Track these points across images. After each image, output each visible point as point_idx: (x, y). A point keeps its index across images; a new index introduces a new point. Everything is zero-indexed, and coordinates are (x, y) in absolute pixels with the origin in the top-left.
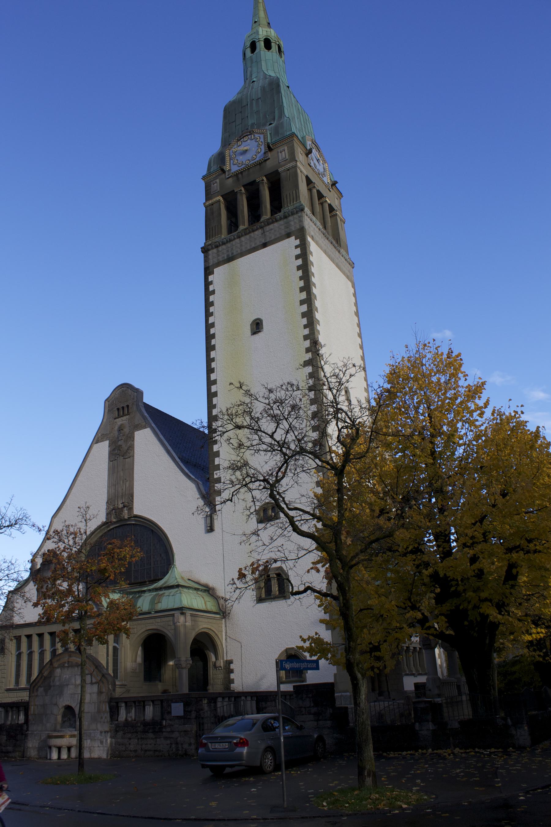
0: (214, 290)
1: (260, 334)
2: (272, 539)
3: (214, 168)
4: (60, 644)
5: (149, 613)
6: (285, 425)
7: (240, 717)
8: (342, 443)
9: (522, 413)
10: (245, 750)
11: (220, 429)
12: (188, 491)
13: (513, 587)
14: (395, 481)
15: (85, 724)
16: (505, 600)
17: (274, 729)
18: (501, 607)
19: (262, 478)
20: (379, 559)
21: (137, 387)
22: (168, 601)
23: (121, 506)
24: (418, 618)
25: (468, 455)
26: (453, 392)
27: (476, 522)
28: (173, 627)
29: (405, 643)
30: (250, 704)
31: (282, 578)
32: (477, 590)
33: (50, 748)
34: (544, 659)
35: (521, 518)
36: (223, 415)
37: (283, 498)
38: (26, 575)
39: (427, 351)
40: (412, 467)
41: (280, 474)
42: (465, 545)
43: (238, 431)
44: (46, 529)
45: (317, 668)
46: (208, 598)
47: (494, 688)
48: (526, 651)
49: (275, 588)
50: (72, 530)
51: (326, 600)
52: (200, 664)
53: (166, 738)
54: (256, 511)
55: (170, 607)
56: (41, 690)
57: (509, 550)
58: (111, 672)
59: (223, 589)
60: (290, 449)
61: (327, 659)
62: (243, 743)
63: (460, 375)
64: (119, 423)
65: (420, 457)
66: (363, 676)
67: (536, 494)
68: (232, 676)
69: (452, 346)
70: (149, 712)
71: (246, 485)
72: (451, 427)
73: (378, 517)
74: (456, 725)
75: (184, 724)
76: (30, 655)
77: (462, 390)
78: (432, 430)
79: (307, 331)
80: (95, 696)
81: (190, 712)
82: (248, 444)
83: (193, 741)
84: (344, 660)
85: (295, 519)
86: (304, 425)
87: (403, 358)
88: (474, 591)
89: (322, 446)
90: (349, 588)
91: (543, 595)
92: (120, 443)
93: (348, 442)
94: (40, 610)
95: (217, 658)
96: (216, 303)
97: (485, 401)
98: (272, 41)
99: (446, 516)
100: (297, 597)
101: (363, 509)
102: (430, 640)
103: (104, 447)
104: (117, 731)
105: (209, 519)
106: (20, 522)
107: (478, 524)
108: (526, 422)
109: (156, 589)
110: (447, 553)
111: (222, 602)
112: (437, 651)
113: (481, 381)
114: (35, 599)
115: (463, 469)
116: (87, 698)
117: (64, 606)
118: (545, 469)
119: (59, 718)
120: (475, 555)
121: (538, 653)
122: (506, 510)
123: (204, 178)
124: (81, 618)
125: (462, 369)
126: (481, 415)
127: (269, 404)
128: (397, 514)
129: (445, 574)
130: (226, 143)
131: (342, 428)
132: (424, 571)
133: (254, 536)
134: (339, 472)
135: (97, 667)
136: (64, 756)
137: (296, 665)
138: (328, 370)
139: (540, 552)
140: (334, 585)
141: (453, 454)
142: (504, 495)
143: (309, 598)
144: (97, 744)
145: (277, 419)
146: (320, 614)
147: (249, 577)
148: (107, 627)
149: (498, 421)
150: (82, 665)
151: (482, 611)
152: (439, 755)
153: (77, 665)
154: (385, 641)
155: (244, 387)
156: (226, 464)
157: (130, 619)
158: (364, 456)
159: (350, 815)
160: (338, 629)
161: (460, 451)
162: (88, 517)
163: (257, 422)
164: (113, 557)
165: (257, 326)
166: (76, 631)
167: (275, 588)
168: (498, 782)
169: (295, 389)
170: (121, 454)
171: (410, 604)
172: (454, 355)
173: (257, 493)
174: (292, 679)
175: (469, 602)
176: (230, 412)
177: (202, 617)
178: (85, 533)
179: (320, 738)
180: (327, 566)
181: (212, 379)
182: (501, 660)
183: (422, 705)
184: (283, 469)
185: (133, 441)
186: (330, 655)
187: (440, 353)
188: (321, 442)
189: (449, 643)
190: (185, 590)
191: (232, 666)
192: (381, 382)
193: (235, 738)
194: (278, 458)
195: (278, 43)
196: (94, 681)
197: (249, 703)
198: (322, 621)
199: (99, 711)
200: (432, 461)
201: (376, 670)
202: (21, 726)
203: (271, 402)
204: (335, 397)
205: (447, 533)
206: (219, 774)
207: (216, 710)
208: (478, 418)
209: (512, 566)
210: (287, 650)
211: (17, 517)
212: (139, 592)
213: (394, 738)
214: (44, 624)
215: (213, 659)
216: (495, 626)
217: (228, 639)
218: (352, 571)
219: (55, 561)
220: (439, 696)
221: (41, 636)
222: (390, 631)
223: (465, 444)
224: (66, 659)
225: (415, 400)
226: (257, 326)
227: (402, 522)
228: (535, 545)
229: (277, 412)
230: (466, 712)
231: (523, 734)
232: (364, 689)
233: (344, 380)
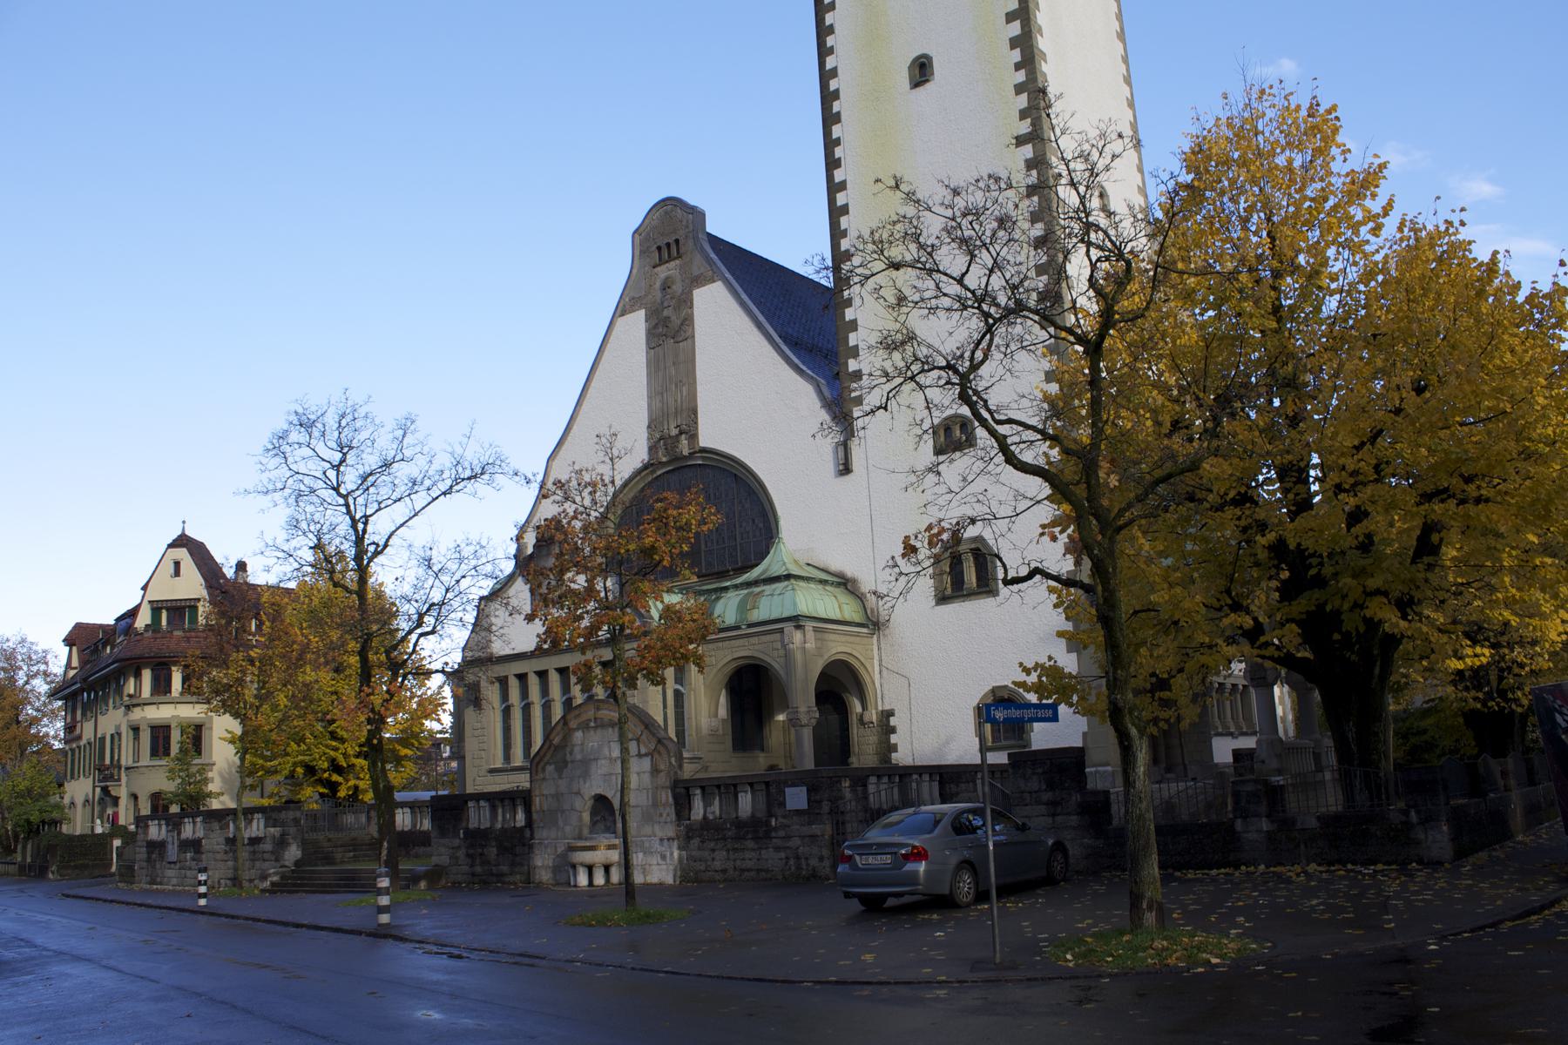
1: (928, 85)
2: (964, 479)
4: (579, 687)
5: (737, 628)
6: (985, 258)
7: (911, 810)
8: (1100, 293)
9: (1463, 224)
10: (922, 867)
11: (859, 271)
12: (800, 398)
13: (1430, 567)
14: (1202, 365)
15: (633, 825)
16: (1413, 593)
17: (974, 830)
18: (1405, 605)
19: (944, 363)
20: (1171, 517)
21: (692, 202)
22: (770, 605)
23: (674, 432)
24: (1246, 626)
25: (1348, 315)
26: (1319, 185)
27: (1363, 444)
28: (782, 652)
29: (1218, 673)
30: (929, 787)
31: (984, 557)
32: (1359, 574)
33: (574, 866)
34: (1484, 704)
35: (1453, 434)
36: (865, 243)
37: (986, 401)
38: (509, 567)
39: (1267, 104)
40: (1234, 338)
41: (979, 355)
42: (1339, 488)
43: (894, 273)
44: (540, 478)
45: (1055, 718)
46: (844, 598)
47: (1387, 758)
48: (1450, 689)
49: (970, 576)
50: (587, 478)
51: (1069, 594)
52: (834, 718)
53: (777, 849)
54: (933, 427)
55: (774, 616)
56: (550, 768)
57: (1427, 497)
58: (672, 733)
59: (870, 577)
60: (998, 305)
61: (1071, 705)
62: (918, 855)
63: (1334, 151)
64: (663, 276)
65: (1251, 316)
66: (1142, 732)
67: (1486, 388)
68: (894, 739)
69: (1318, 93)
70: (746, 803)
71: (912, 378)
72: (1315, 256)
73: (1169, 436)
74: (1312, 823)
75: (810, 824)
76: (527, 709)
77: (1338, 182)
78: (1275, 264)
79: (1021, 76)
80: (646, 778)
81: (820, 802)
82: (916, 297)
83: (826, 852)
84: (1103, 705)
85: (1009, 441)
86: (1022, 258)
87: (1218, 119)
88: (1354, 577)
89: (1058, 298)
90: (1114, 569)
91: (1488, 584)
92: (666, 313)
93: (1108, 293)
94: (538, 627)
95: (864, 707)
97: (1384, 203)
99: (1301, 433)
100: (1015, 587)
101: (1139, 422)
102: (1265, 670)
103: (637, 322)
104: (688, 838)
105: (841, 449)
106: (489, 469)
107: (1368, 446)
108: (1470, 243)
109: (748, 584)
110: (1302, 505)
111: (872, 599)
112: (1277, 690)
113: (1377, 162)
114: (527, 609)
115: (1338, 340)
116: (634, 781)
117: (581, 618)
118: (1506, 337)
119: (586, 817)
120: (1358, 507)
121: (1473, 693)
122: (1423, 420)
124: (613, 641)
125: (1339, 139)
126: (1376, 231)
127: (953, 219)
128: (1206, 430)
129: (1299, 545)
131: (1098, 260)
132: (1258, 538)
133: (931, 475)
134: (1094, 349)
135: (647, 727)
136: (599, 880)
137: (1015, 713)
138: (1068, 145)
139: (1487, 500)
140: (1087, 563)
141: (1318, 309)
142: (1419, 390)
143: (1038, 590)
144: (655, 860)
145: (970, 247)
146: (1059, 621)
147: (924, 552)
148: (662, 653)
149: (1412, 242)
150: (621, 724)
151: (1368, 613)
152: (1279, 876)
153: (612, 725)
154: (1181, 670)
155: (902, 187)
156: (874, 339)
157: (703, 639)
158: (1143, 316)
159: (1116, 975)
160: (1092, 649)
161: (1331, 304)
162: (616, 452)
163: (930, 254)
164: (666, 525)
165: (922, 71)
166: (605, 664)
167: (970, 576)
168: (1390, 921)
169: (1003, 186)
170: (669, 332)
171: (1229, 601)
172: (1321, 110)
173: (934, 394)
174: (1004, 743)
175: (1344, 597)
176: (877, 236)
177: (834, 631)
178: (613, 482)
179: (1059, 846)
180: (1070, 531)
182: (1400, 707)
183: (1250, 788)
184: (984, 344)
185: (691, 307)
186: (1075, 698)
187: (1293, 107)
188: (1052, 296)
189: (1300, 672)
190: (802, 584)
191: (893, 721)
192: (1176, 165)
193: (906, 845)
194: (976, 324)
196: (643, 751)
197: (925, 787)
198: (1060, 634)
199: (655, 805)
200: (1275, 325)
201: (1161, 724)
202: (521, 829)
203: (958, 214)
204: (1082, 199)
205: (1302, 464)
206: (874, 906)
207: (866, 798)
208: (1369, 237)
209: (1429, 528)
210: (994, 690)
211: (484, 460)
212: (715, 590)
213: (1197, 845)
214: (545, 653)
215: (859, 709)
216: (1392, 641)
217: (885, 672)
218: (1119, 538)
219: (559, 536)
220: (1280, 772)
221: (542, 675)
222: (1190, 651)
223: (1341, 292)
224: (591, 714)
225: (1242, 205)
226: (922, 71)
227: (1215, 443)
228: (1479, 488)
229: (967, 233)
230: (1332, 800)
231: (1439, 839)
232: (1142, 756)
233: (1100, 166)
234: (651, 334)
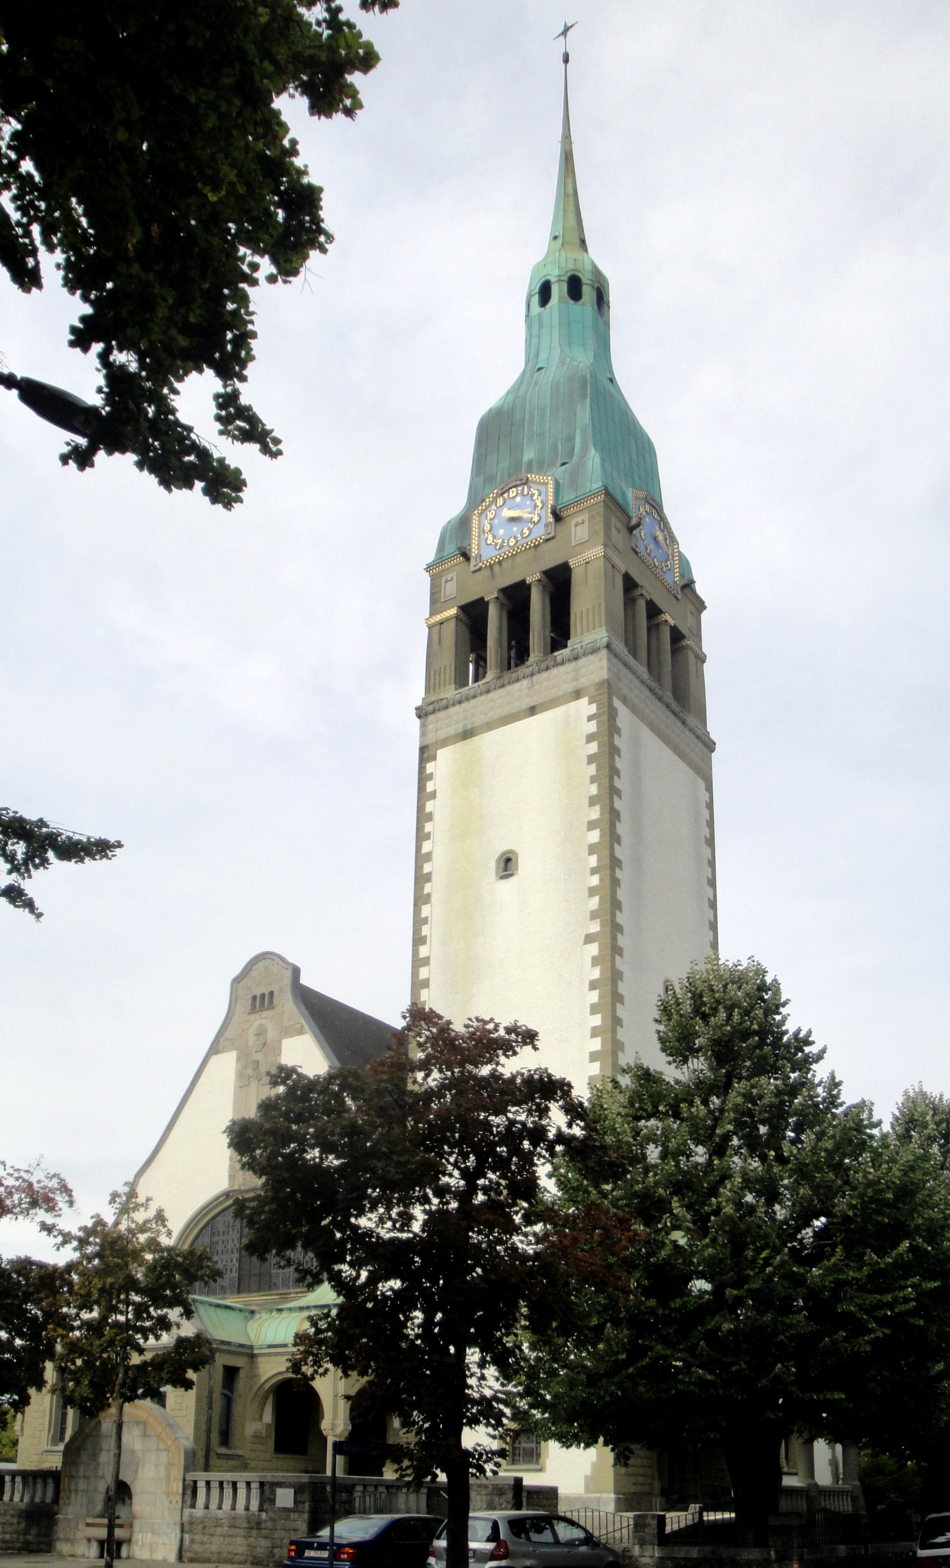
0: (434, 792)
3: (451, 549)
64: (257, 1023)
96: (436, 817)
98: (584, 280)
123: (429, 568)
130: (476, 499)
165: (507, 864)
181: (421, 956)
195: (596, 285)
234: (240, 1075)
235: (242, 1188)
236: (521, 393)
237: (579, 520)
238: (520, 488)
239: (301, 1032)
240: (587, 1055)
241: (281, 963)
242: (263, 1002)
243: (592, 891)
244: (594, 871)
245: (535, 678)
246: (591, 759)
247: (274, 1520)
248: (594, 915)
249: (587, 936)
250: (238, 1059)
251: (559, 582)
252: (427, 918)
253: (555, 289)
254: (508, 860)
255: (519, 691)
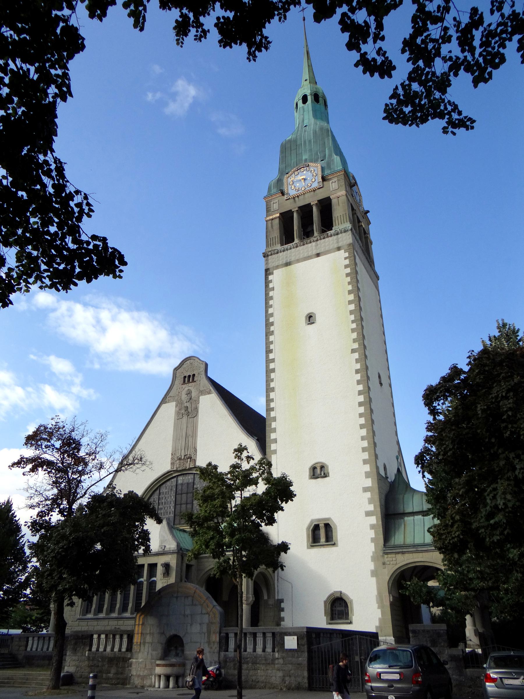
64: (186, 389)
68: (283, 614)
96: (275, 298)
103: (170, 410)
130: (284, 172)
165: (310, 319)
170: (188, 412)
226: (310, 319)
234: (178, 413)
235: (178, 469)
236: (298, 134)
237: (334, 181)
238: (305, 168)
239: (209, 393)
240: (357, 404)
241: (199, 361)
242: (189, 379)
243: (353, 330)
244: (353, 322)
245: (318, 242)
246: (347, 275)
247: (283, 658)
248: (354, 341)
249: (352, 350)
250: (176, 406)
251: (326, 206)
252: (272, 341)
253: (309, 98)
254: (310, 317)
255: (311, 247)
